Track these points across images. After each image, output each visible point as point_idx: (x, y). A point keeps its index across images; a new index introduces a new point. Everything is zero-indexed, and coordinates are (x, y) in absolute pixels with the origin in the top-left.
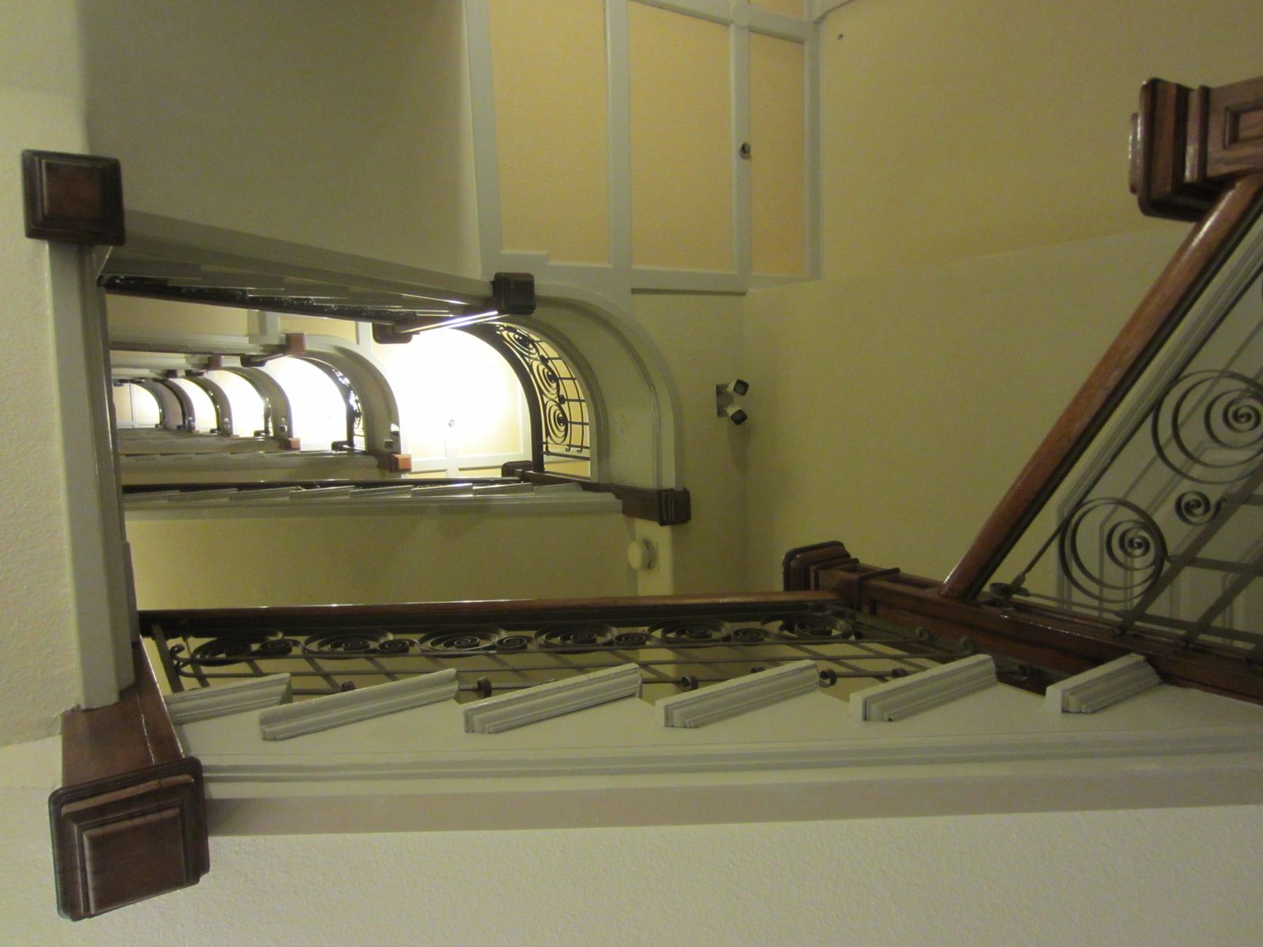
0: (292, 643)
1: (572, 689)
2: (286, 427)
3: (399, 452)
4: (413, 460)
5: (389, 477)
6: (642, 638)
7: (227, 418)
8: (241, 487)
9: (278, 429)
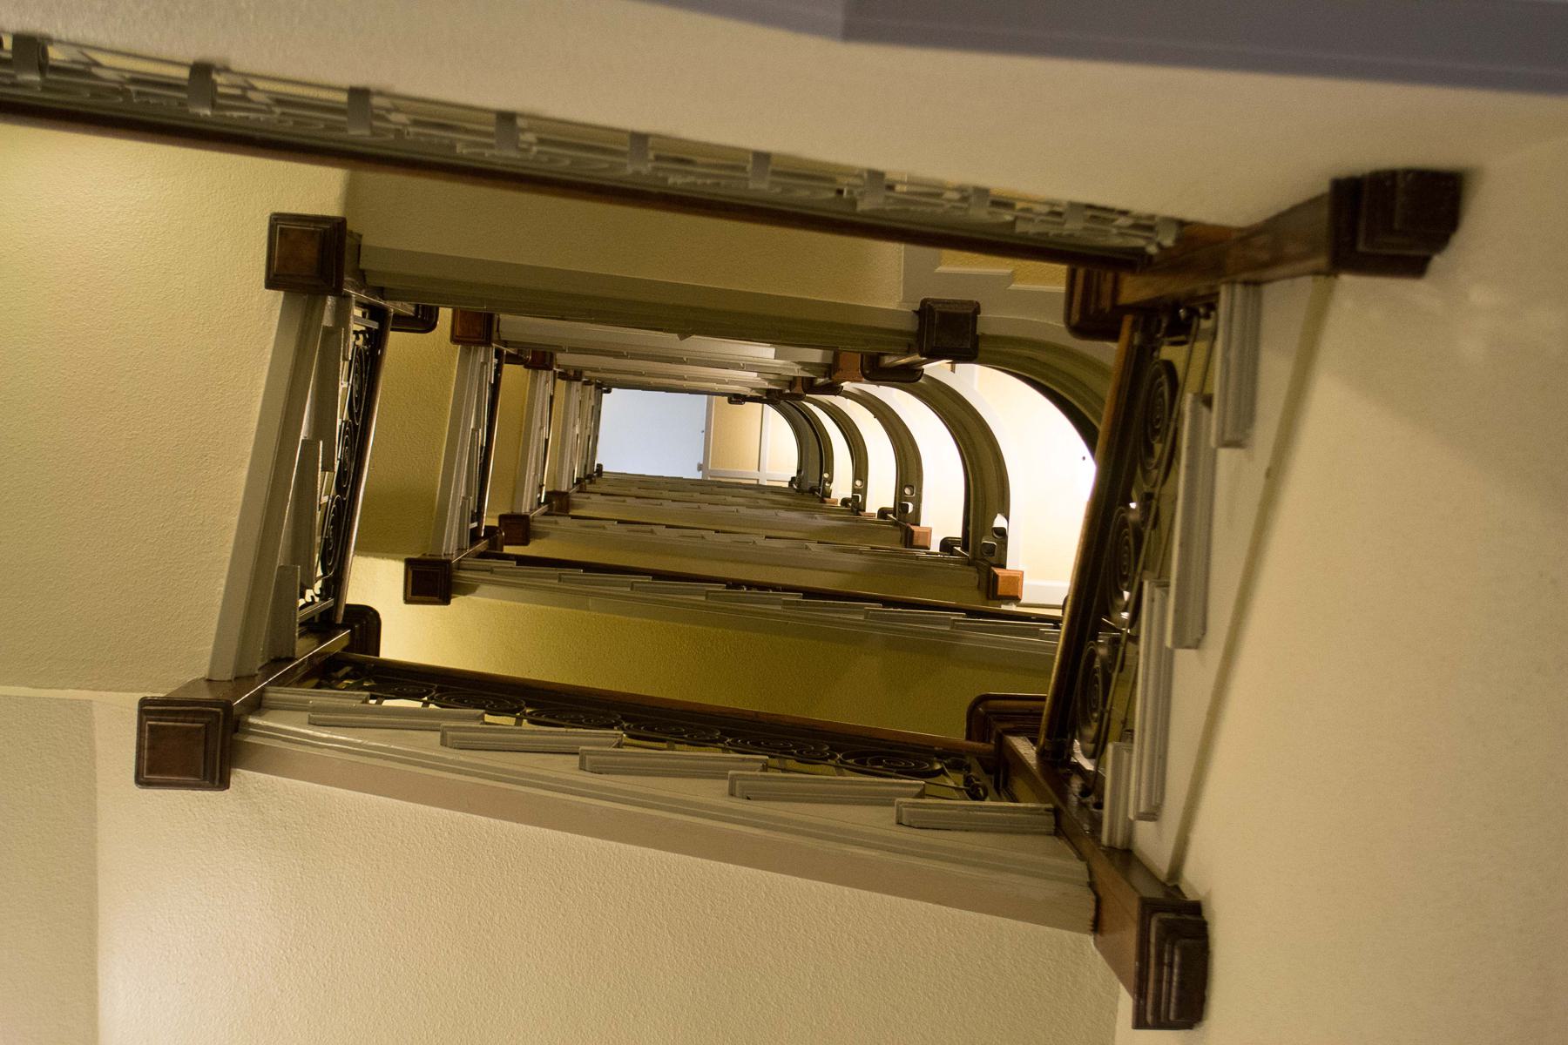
0: (524, 703)
1: (529, 734)
2: (911, 506)
3: (1003, 566)
4: (1026, 582)
5: (991, 607)
6: (586, 721)
7: (861, 480)
8: (658, 575)
9: (900, 506)
